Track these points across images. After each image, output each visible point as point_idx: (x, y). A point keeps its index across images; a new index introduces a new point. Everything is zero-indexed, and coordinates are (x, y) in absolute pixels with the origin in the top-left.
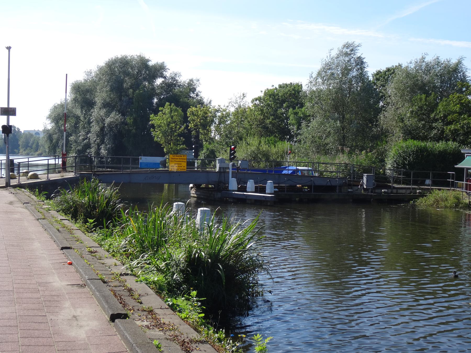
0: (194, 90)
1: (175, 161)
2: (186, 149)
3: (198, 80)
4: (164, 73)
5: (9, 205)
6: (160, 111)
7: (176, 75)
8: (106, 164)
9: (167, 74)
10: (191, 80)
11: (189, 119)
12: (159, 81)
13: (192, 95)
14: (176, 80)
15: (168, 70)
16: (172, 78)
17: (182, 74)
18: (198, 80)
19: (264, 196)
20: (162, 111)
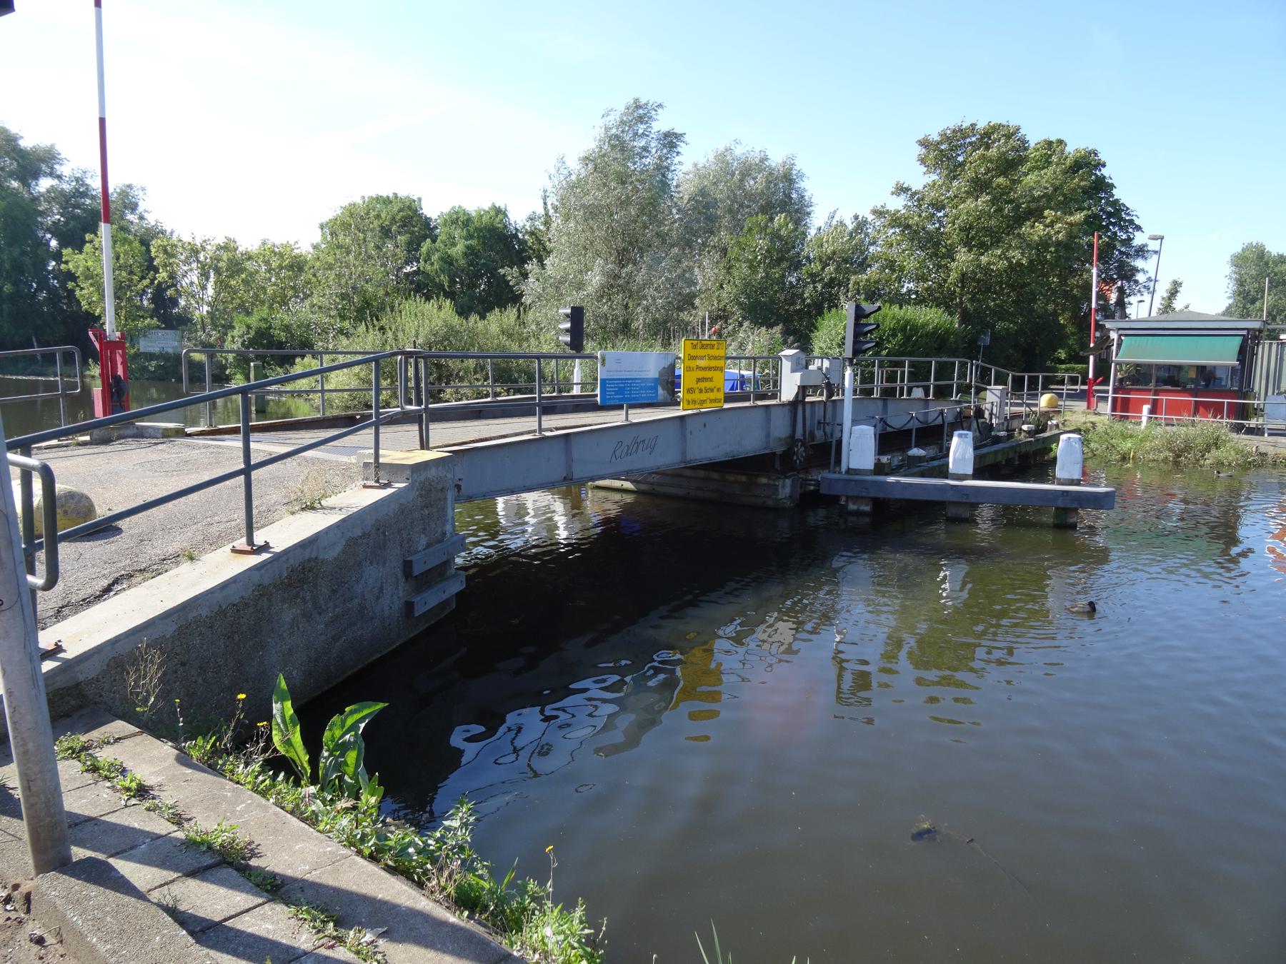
0: (133, 207)
1: (698, 368)
2: (159, 327)
3: (143, 189)
4: (57, 167)
5: (890, 684)
6: (88, 242)
7: (85, 172)
8: (532, 391)
9: (64, 170)
10: (130, 186)
11: (155, 263)
12: (44, 184)
13: (130, 217)
14: (87, 185)
15: (65, 162)
16: (77, 180)
17: (916, 157)
18: (143, 189)
19: (916, 436)
20: (91, 242)
